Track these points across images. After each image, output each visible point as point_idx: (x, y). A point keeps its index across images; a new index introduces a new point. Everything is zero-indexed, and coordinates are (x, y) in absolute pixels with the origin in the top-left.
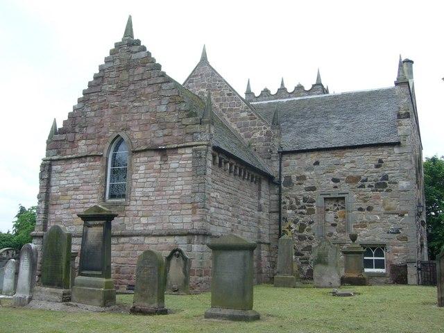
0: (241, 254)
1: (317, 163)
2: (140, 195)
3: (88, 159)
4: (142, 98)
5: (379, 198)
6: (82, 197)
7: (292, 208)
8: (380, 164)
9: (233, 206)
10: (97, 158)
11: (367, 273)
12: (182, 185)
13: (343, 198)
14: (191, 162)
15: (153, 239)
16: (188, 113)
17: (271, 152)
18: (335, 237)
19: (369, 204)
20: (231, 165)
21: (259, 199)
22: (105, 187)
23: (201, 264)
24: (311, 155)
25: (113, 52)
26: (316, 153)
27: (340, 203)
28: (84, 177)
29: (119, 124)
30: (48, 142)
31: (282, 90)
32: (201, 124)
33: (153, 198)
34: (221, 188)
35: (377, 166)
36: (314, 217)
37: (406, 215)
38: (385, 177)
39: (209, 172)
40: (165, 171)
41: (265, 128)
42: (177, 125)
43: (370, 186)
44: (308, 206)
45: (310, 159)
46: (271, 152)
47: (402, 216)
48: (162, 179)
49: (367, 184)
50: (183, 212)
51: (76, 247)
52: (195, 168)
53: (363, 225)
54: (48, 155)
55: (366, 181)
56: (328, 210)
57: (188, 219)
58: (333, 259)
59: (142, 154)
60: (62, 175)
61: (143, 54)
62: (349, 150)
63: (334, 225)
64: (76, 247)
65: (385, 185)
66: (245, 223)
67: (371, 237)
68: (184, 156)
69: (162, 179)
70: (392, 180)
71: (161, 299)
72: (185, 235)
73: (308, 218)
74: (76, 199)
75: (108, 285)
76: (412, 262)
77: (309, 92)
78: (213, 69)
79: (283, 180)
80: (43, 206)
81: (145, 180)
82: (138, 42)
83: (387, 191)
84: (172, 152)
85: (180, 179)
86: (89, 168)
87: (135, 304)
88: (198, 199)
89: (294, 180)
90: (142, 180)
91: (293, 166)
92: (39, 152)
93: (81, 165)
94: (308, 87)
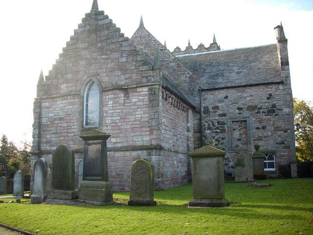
0: (215, 159)
1: (226, 97)
2: (110, 122)
3: (69, 97)
4: (108, 52)
5: (269, 120)
6: (66, 125)
7: (209, 129)
8: (270, 97)
9: (173, 128)
10: (76, 96)
11: (267, 171)
12: (141, 115)
13: (246, 121)
14: (148, 97)
15: (121, 153)
16: (143, 62)
17: (193, 90)
18: (240, 148)
19: (264, 124)
20: (172, 99)
21: (187, 123)
22: (83, 117)
23: (159, 170)
24: (222, 91)
25: (84, 20)
26: (226, 90)
27: (243, 124)
28: (66, 110)
29: (91, 72)
30: (38, 86)
31: (189, 48)
32: (153, 70)
33: (120, 124)
34: (167, 115)
35: (268, 99)
36: (225, 135)
37: (289, 131)
38: (274, 106)
39: (161, 104)
40: (128, 104)
41: (188, 73)
42: (135, 70)
43: (263, 112)
44: (221, 127)
45: (221, 94)
46: (193, 90)
47: (286, 132)
48: (127, 110)
49: (261, 111)
50: (143, 133)
51: (78, 160)
52: (150, 101)
53: (260, 139)
54: (38, 95)
55: (261, 108)
56: (235, 130)
57: (147, 138)
58: (248, 162)
59: (110, 93)
60: (50, 109)
61: (106, 21)
62: (248, 88)
63: (239, 140)
64: (78, 160)
65: (274, 111)
66: (180, 140)
67: (265, 147)
68: (141, 93)
69: (127, 110)
70: (279, 107)
71: (152, 196)
72: (146, 149)
73: (221, 135)
74: (61, 127)
75: (107, 187)
76: (293, 163)
77: (208, 49)
78: (148, 31)
79: (202, 109)
80: (37, 132)
81: (113, 111)
82: (102, 13)
83: (276, 115)
84: (132, 90)
85: (139, 110)
86: (71, 104)
87: (132, 199)
88: (154, 124)
89: (211, 109)
90: (111, 112)
91: (210, 100)
92: (33, 94)
93: (64, 102)
94: (207, 46)
